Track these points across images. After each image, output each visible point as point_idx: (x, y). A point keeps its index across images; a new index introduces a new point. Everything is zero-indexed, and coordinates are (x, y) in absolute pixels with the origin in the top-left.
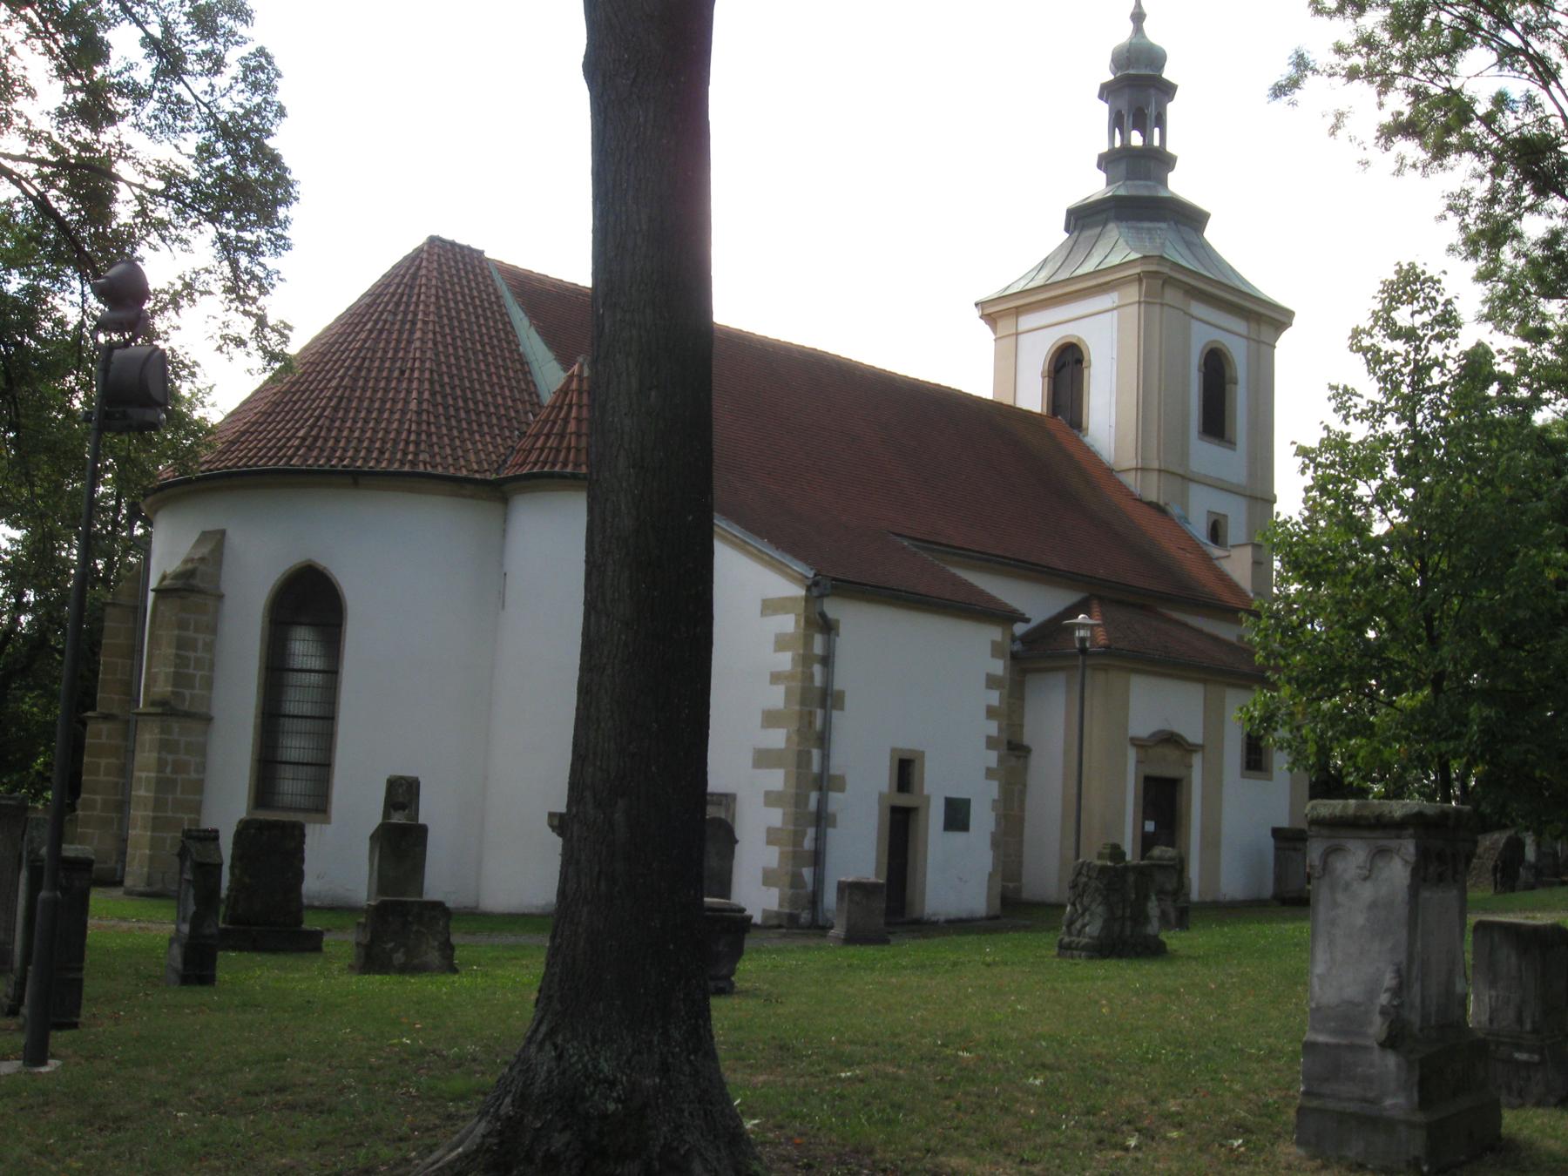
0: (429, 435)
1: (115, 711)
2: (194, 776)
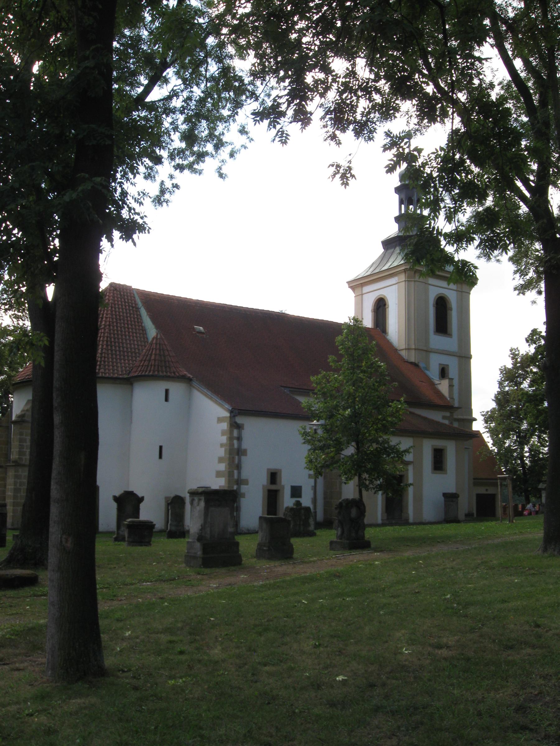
0: (105, 362)
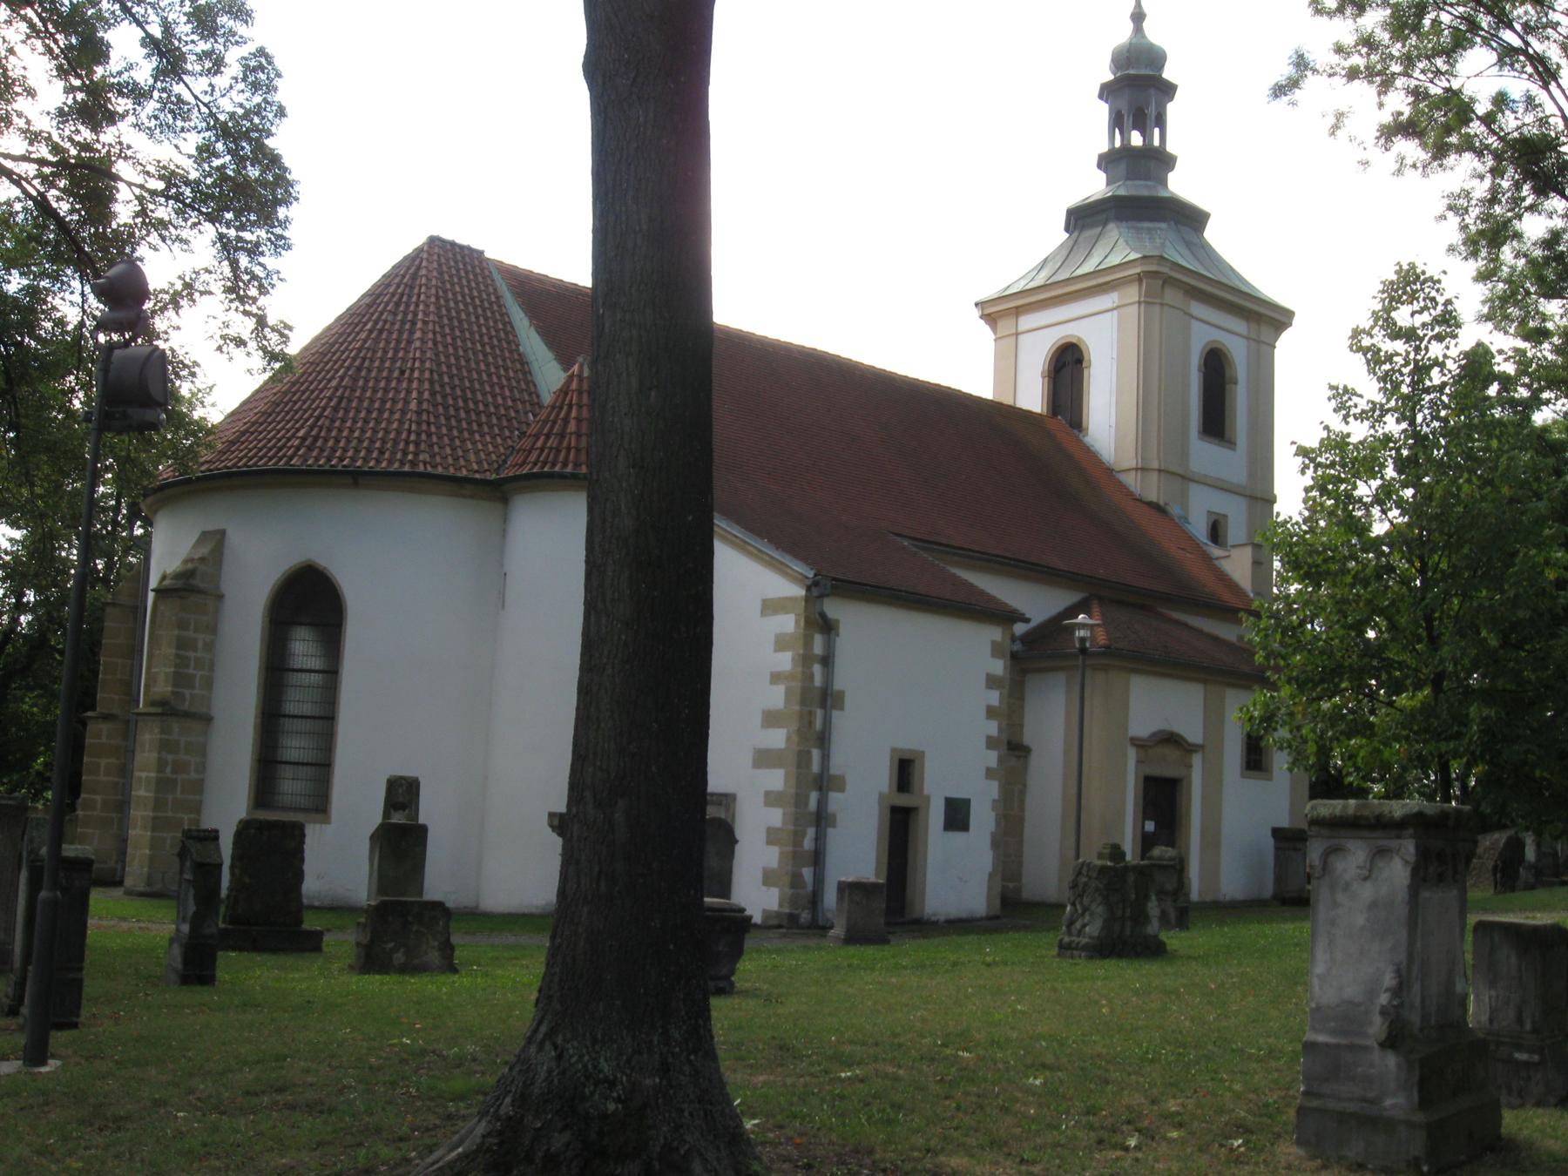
0: (429, 435)
1: (115, 711)
2: (194, 776)
